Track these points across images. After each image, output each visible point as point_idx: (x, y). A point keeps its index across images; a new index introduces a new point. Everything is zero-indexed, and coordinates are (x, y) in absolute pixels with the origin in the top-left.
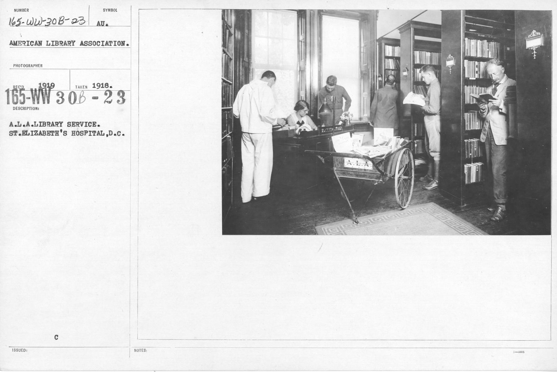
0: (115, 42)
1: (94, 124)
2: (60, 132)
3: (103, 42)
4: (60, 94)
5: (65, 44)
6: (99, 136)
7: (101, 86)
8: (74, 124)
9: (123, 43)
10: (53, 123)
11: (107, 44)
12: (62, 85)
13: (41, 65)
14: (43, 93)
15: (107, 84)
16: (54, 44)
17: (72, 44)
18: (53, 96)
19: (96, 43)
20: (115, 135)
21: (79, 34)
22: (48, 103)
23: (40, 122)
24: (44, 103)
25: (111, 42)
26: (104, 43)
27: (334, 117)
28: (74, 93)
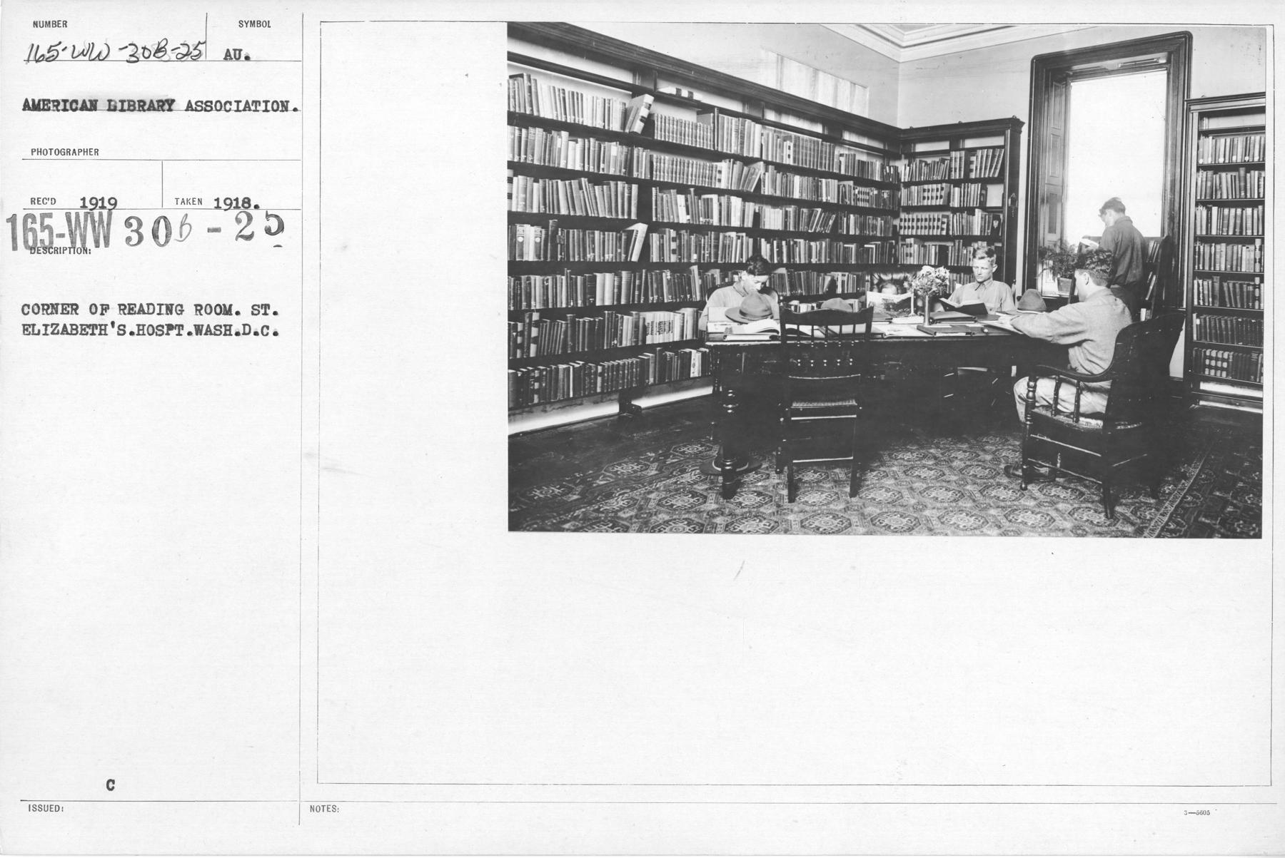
0: (266, 102)
1: (167, 308)
3: (238, 102)
7: (100, 204)
8: (128, 309)
9: (284, 106)
12: (139, 197)
13: (97, 151)
14: (94, 221)
15: (247, 201)
16: (126, 106)
17: (166, 107)
18: (119, 231)
19: (223, 106)
20: (256, 334)
22: (107, 244)
24: (97, 246)
25: (256, 103)
26: (242, 106)
28: (165, 218)
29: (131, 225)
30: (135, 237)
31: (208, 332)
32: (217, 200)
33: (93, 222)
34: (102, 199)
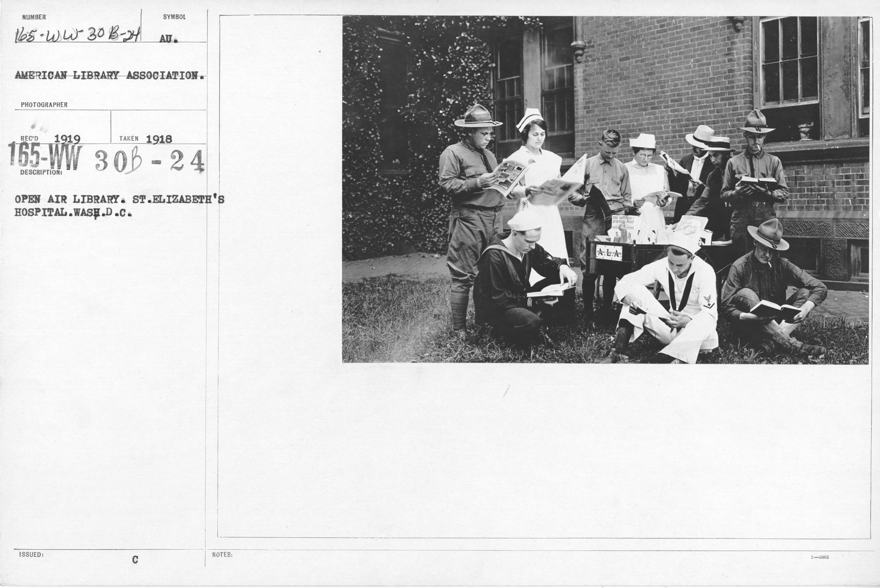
0: (182, 73)
2: (213, 197)
3: (163, 72)
4: (101, 154)
5: (103, 76)
6: (84, 217)
7: (160, 140)
9: (194, 75)
10: (103, 197)
11: (169, 76)
13: (66, 104)
14: (66, 150)
17: (113, 77)
19: (152, 75)
20: (117, 215)
21: (125, 57)
22: (75, 168)
23: (84, 196)
25: (176, 73)
27: (482, 208)
28: (123, 153)
29: (99, 156)
30: (102, 164)
31: (84, 213)
32: (149, 137)
33: (67, 152)
34: (70, 136)
